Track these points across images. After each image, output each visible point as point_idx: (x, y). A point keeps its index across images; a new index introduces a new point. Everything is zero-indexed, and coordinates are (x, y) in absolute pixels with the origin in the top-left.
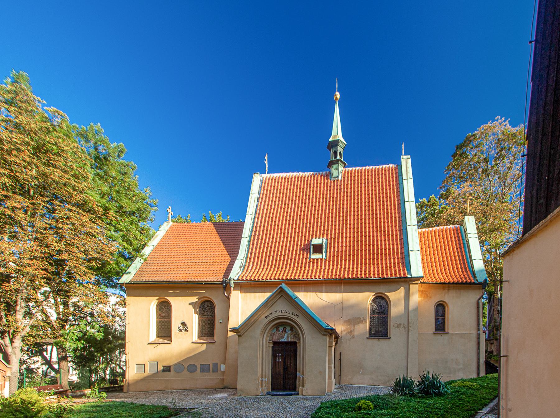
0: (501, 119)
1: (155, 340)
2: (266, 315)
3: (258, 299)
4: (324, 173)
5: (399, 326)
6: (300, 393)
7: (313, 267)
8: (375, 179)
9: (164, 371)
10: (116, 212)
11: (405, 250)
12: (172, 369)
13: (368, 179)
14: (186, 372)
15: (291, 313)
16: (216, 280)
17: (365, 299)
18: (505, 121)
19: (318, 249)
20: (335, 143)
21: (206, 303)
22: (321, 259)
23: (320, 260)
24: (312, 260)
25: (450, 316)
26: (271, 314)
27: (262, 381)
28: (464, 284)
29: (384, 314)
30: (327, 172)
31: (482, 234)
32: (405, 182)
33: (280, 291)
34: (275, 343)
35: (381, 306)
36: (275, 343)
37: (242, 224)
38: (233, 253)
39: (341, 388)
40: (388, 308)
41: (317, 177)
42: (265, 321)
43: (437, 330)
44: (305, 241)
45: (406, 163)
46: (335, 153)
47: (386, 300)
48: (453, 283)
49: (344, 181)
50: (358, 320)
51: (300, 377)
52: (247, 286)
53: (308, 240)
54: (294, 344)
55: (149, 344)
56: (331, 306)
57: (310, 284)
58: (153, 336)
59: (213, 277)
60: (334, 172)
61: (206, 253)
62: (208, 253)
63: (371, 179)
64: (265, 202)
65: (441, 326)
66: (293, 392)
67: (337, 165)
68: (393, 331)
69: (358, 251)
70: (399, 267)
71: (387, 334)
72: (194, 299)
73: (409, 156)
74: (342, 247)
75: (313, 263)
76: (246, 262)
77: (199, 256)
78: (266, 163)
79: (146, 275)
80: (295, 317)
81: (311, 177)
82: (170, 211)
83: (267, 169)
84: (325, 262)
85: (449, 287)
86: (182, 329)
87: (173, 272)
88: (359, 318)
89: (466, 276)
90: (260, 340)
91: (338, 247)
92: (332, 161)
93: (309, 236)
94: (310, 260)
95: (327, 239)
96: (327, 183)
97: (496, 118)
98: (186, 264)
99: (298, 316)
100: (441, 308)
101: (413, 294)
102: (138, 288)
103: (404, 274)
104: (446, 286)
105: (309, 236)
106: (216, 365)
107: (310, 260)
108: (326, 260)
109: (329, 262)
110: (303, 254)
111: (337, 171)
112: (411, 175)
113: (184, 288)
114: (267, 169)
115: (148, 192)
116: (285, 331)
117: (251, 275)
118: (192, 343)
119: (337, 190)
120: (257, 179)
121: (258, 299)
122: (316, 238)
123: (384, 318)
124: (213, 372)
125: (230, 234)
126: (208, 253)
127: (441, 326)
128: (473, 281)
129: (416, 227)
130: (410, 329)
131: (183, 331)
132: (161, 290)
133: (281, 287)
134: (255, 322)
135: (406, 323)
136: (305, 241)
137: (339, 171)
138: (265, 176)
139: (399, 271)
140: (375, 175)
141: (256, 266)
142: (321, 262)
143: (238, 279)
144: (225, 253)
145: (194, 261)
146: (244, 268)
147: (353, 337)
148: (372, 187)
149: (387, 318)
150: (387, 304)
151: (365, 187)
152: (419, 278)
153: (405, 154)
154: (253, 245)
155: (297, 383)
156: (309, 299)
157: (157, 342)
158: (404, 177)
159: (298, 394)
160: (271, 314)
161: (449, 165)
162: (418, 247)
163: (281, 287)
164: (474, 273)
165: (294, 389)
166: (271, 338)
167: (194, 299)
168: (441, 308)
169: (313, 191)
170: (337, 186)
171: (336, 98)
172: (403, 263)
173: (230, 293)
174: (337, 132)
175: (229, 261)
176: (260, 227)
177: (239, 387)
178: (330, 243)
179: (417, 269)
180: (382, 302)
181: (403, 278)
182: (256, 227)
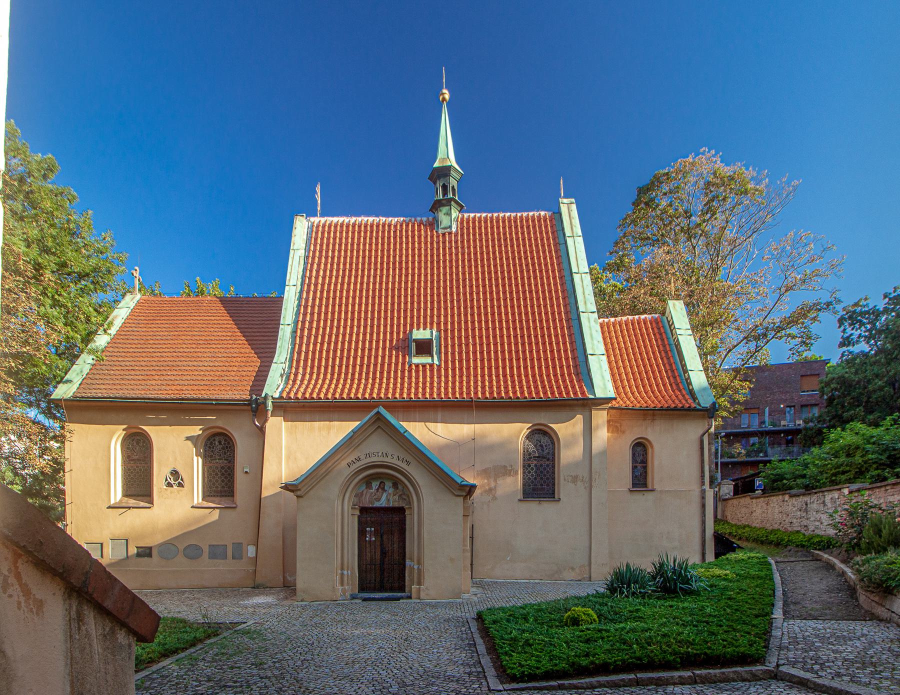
0: (709, 152)
1: (121, 501)
2: (349, 460)
3: (331, 434)
4: (424, 219)
5: (575, 479)
6: (414, 595)
7: (417, 378)
8: (517, 234)
9: (139, 555)
10: (53, 272)
11: (579, 353)
12: (154, 552)
13: (505, 234)
14: (181, 558)
15: (395, 457)
16: (238, 397)
17: (513, 433)
18: (714, 156)
19: (424, 347)
20: (445, 172)
21: (217, 439)
22: (432, 365)
23: (428, 367)
24: (414, 367)
25: (656, 463)
26: (359, 459)
27: (342, 574)
28: (680, 410)
29: (548, 460)
30: (431, 219)
31: (699, 328)
32: (570, 241)
33: (377, 418)
34: (363, 510)
35: (541, 446)
36: (363, 510)
37: (278, 302)
38: (266, 354)
39: (480, 585)
40: (554, 449)
41: (413, 226)
42: (348, 472)
43: (634, 485)
44: (398, 333)
45: (570, 212)
46: (445, 188)
47: (550, 437)
48: (662, 409)
49: (462, 235)
50: (505, 471)
51: (412, 568)
52: (296, 409)
53: (405, 332)
54: (401, 511)
55: (109, 507)
56: (456, 446)
57: (415, 407)
58: (117, 493)
59: (230, 393)
60: (444, 220)
61: (212, 350)
62: (217, 350)
63: (511, 234)
64: (319, 265)
65: (640, 479)
66: (399, 594)
67: (448, 208)
68: (564, 488)
69: (496, 352)
70: (571, 381)
71: (554, 493)
72: (196, 431)
73: (573, 200)
74: (467, 345)
75: (417, 372)
76: (291, 367)
77: (200, 355)
78: (318, 197)
79: (102, 387)
80: (404, 465)
81: (401, 226)
82: (137, 274)
83: (319, 208)
84: (439, 370)
85: (654, 415)
86: (172, 482)
87: (154, 382)
88: (505, 467)
89: (680, 397)
90: (338, 504)
91: (460, 345)
92: (440, 200)
93: (405, 325)
94: (410, 366)
95: (439, 330)
96: (432, 237)
97: (701, 150)
98: (177, 368)
99: (408, 463)
100: (640, 450)
101: (597, 427)
102: (88, 408)
103: (583, 393)
104: (649, 414)
105: (405, 325)
107: (410, 366)
108: (439, 366)
109: (446, 370)
110: (397, 357)
111: (448, 218)
112: (578, 230)
113: (176, 410)
114: (319, 208)
115: (108, 239)
116: (382, 487)
117: (303, 390)
118: (193, 507)
119: (450, 248)
120: (301, 227)
121: (331, 434)
122: (418, 329)
123: (548, 466)
125: (255, 320)
126: (217, 350)
127: (640, 479)
128: (693, 405)
129: (596, 315)
130: (593, 484)
131: (175, 487)
132: (134, 413)
133: (378, 412)
134: (327, 473)
135: (586, 475)
136: (398, 333)
137: (451, 219)
138: (316, 220)
139: (573, 387)
140: (516, 227)
141: (311, 374)
142: (432, 371)
143: (281, 397)
144: (248, 351)
145: (191, 364)
146: (288, 378)
147: (495, 498)
148: (512, 246)
149: (554, 467)
150: (553, 443)
151: (500, 246)
152: (608, 400)
153: (566, 197)
154: (301, 338)
155: (407, 578)
156: (426, 433)
157: (124, 505)
158: (568, 232)
159: (410, 597)
160: (359, 459)
161: (626, 219)
162: (601, 349)
163: (378, 412)
164: (692, 393)
165: (402, 589)
166: (356, 500)
167: (196, 431)
168: (640, 450)
169: (407, 250)
170: (450, 242)
171: (444, 99)
172: (577, 375)
173: (266, 421)
174: (447, 152)
175: (259, 364)
176: (313, 307)
177: (300, 585)
178: (446, 339)
179: (603, 384)
180: (545, 440)
181: (581, 399)
182: (306, 307)
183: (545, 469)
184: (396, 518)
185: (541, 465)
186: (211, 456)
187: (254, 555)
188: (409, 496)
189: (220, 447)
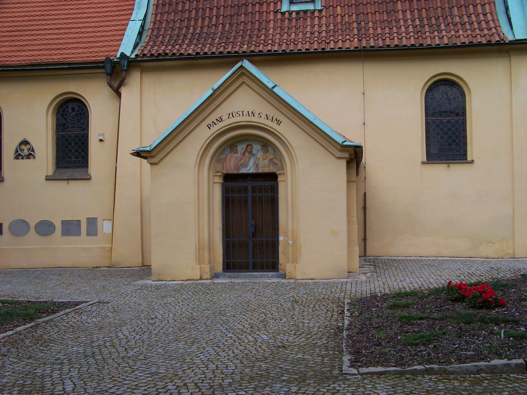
15: (263, 116)
21: (70, 105)
29: (457, 115)
34: (228, 178)
36: (228, 178)
54: (273, 177)
99: (279, 122)
106: (92, 222)
123: (457, 122)
124: (88, 234)
133: (242, 66)
160: (221, 120)
163: (242, 66)
183: (453, 126)
184: (268, 184)
185: (449, 122)
186: (64, 125)
187: (110, 231)
188: (282, 160)
189: (74, 114)
